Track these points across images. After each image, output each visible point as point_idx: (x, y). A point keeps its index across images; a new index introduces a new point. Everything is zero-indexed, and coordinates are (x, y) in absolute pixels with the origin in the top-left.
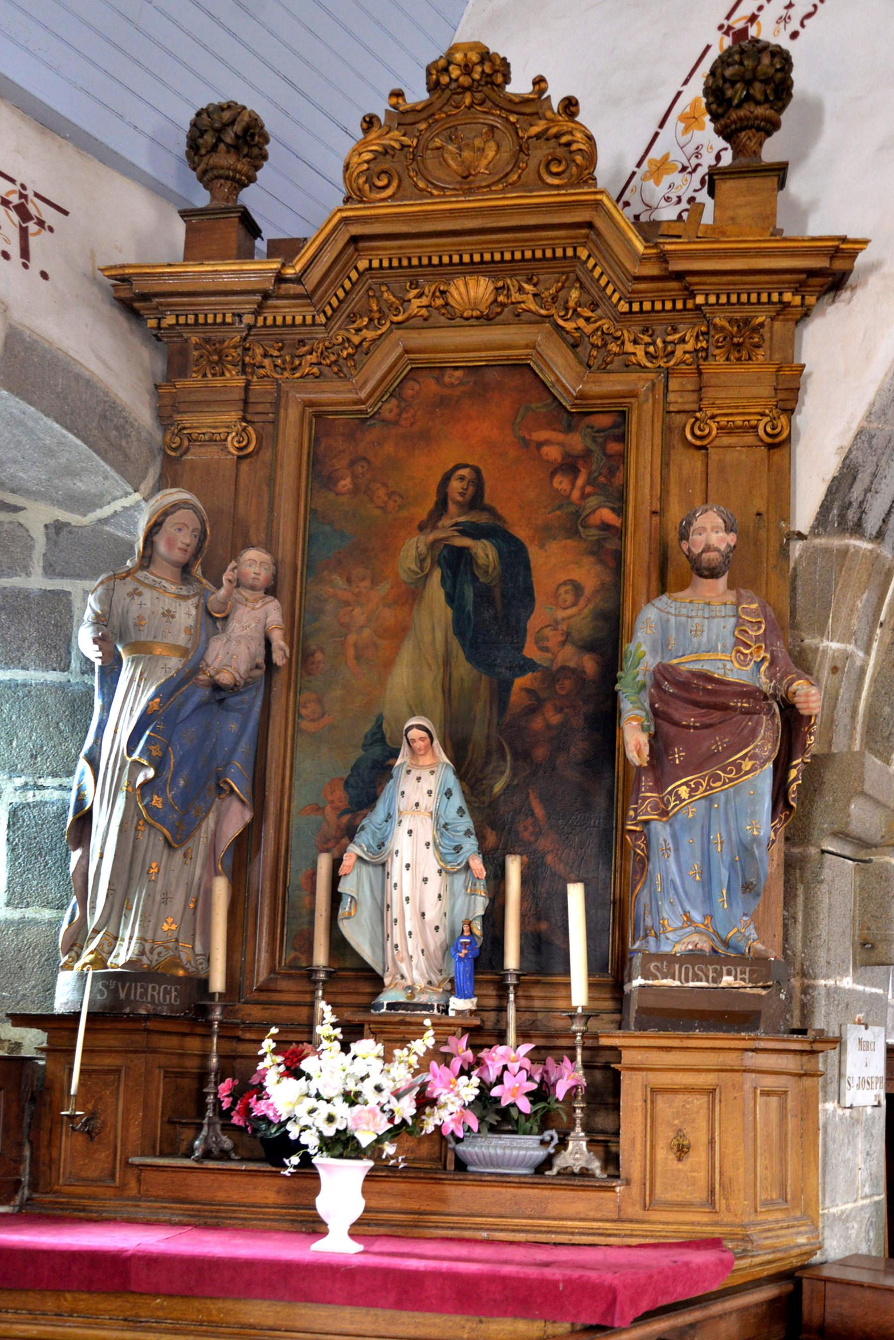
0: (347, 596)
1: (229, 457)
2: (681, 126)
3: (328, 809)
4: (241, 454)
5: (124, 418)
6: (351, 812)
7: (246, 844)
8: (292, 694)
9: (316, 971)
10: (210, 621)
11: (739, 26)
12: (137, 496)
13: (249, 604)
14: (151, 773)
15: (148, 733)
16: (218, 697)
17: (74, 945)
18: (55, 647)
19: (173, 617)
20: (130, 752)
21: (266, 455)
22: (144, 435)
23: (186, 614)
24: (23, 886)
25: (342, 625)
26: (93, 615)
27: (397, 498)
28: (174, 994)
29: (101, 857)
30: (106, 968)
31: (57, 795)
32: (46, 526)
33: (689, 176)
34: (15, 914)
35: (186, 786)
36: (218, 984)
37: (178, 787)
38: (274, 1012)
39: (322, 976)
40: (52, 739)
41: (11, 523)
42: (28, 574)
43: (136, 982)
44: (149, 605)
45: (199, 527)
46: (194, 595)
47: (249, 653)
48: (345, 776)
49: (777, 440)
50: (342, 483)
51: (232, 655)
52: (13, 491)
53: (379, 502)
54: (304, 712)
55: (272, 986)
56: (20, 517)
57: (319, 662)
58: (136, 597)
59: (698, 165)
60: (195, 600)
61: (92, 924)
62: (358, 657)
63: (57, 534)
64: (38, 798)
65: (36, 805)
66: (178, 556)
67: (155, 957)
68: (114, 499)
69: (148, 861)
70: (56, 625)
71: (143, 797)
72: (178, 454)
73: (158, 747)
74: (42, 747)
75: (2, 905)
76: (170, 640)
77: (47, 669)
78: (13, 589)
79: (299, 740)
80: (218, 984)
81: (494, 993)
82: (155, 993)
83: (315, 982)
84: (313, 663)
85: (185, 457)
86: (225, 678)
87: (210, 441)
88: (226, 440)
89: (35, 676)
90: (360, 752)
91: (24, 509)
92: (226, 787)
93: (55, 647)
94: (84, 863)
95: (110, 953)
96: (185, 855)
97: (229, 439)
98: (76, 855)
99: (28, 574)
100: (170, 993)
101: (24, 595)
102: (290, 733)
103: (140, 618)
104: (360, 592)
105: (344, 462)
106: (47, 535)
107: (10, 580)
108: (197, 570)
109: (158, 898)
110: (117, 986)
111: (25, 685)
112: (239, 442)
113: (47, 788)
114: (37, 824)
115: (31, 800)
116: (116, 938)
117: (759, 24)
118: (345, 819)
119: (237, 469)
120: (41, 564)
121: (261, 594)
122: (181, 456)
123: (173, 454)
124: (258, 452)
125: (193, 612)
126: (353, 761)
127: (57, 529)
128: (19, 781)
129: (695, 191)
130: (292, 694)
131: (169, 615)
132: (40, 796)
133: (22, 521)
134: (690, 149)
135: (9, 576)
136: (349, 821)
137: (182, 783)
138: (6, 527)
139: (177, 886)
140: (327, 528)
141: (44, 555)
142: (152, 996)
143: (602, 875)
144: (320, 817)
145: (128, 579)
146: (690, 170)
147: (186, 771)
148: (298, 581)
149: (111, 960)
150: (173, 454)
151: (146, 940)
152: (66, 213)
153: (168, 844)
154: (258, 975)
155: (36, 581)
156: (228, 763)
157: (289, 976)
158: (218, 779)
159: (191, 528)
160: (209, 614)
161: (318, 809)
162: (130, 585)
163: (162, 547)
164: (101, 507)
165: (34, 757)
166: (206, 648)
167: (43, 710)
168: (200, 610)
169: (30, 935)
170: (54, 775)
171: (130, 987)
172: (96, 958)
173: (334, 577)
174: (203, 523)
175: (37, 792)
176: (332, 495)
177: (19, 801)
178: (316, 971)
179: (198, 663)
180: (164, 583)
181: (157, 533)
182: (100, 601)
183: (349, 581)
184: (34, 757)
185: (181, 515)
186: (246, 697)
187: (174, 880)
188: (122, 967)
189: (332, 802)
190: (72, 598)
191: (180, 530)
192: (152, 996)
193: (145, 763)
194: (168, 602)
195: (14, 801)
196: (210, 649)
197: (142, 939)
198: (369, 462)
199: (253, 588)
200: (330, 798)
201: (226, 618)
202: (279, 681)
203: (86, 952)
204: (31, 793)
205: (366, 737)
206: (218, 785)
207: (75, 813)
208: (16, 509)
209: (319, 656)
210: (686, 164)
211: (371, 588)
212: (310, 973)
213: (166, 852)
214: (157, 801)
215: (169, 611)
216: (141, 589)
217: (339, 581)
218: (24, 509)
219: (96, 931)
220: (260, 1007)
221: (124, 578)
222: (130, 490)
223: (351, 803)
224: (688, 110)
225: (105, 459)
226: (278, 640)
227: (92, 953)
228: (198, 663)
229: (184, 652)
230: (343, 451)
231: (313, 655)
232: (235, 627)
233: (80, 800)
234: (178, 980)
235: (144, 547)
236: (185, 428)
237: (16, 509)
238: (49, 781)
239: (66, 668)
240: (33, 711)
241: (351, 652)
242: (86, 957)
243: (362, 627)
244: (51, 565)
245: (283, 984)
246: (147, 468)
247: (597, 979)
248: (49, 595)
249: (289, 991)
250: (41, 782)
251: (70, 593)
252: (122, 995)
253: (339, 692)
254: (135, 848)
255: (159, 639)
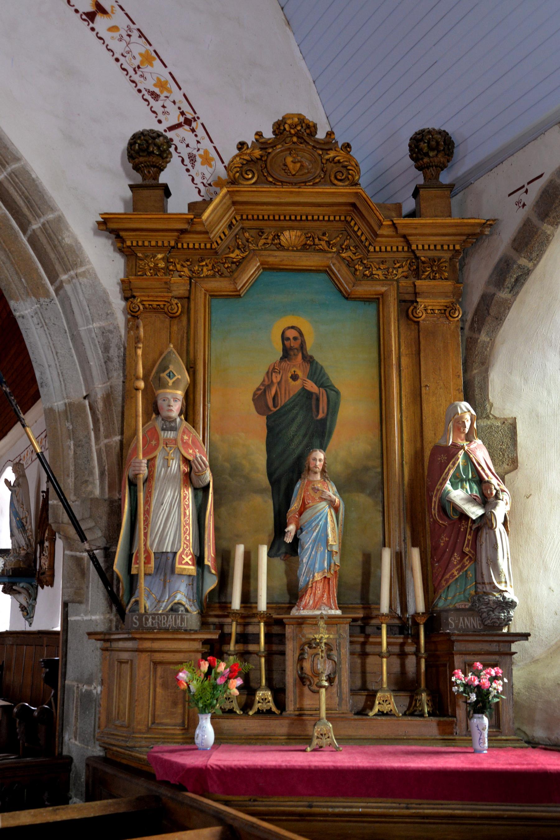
2: (163, 79)
11: (194, 125)
33: (134, 67)
49: (174, 315)
59: (136, 73)
81: (99, 389)
117: (189, 131)
129: (122, 64)
134: (147, 75)
143: (501, 762)
146: (137, 69)
152: (510, 195)
210: (140, 70)
224: (168, 86)
247: (243, 605)
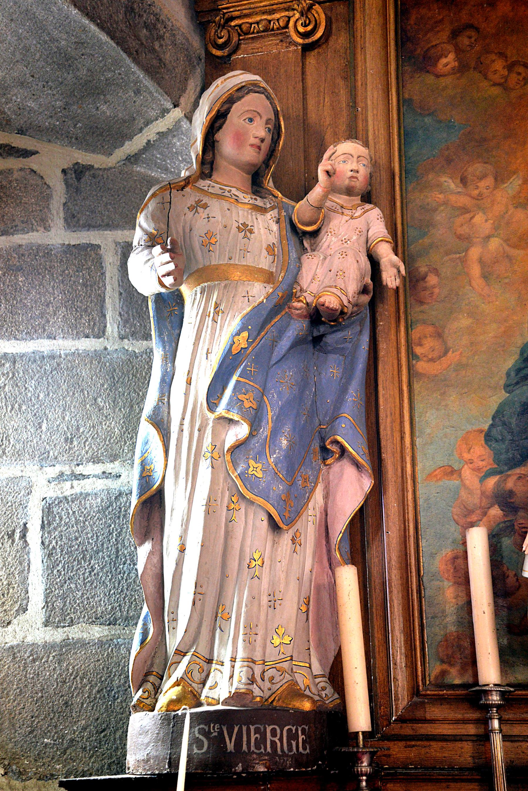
0: (464, 200)
1: (293, 48)
3: (467, 473)
4: (307, 41)
5: (155, 15)
6: (501, 472)
7: (364, 525)
8: (402, 329)
9: (487, 693)
10: (293, 240)
12: (177, 113)
13: (346, 212)
14: (242, 431)
15: (235, 378)
16: (316, 334)
17: (148, 674)
18: (86, 311)
19: (251, 231)
20: (212, 406)
21: (339, 41)
22: (179, 39)
23: (267, 228)
24: (64, 598)
25: (459, 237)
26: (145, 237)
27: (521, 69)
28: (301, 737)
29: (182, 550)
30: (200, 705)
31: (101, 484)
32: (64, 171)
34: (56, 635)
35: (291, 447)
36: (360, 719)
37: (280, 449)
38: (423, 751)
39: (495, 698)
40: (89, 419)
41: (21, 170)
42: (47, 229)
43: (248, 725)
44: (219, 218)
45: (273, 118)
46: (272, 208)
47: (359, 269)
48: (486, 427)
50: (444, 61)
51: (333, 274)
52: (21, 132)
53: (496, 78)
54: (418, 350)
55: (419, 714)
56: (32, 163)
57: (434, 287)
58: (200, 210)
60: (274, 213)
61: (173, 641)
62: (485, 276)
63: (79, 179)
64: (77, 490)
65: (75, 498)
66: (250, 155)
67: (267, 684)
68: (147, 123)
69: (247, 550)
70: (85, 285)
71: (235, 464)
72: (226, 52)
73: (250, 395)
74: (78, 429)
75: (40, 624)
76: (249, 261)
77: (78, 336)
78: (30, 246)
79: (416, 386)
80: (360, 719)
82: (276, 740)
83: (487, 707)
84: (425, 289)
85: (234, 57)
86: (331, 301)
87: (266, 30)
88: (286, 26)
89: (65, 345)
90: (502, 396)
91: (37, 152)
92: (334, 448)
93: (86, 311)
94: (155, 559)
95: (204, 683)
96: (293, 540)
97: (291, 24)
98: (144, 551)
99: (47, 229)
100: (295, 737)
101: (46, 252)
102: (405, 378)
103: (209, 235)
104: (480, 195)
105: (445, 35)
106: (66, 182)
107: (26, 236)
108: (269, 184)
109: (265, 600)
110: (221, 733)
111: (52, 357)
112: (305, 25)
113: (88, 477)
114: (77, 522)
115: (68, 493)
116: (210, 661)
118: (492, 482)
119: (303, 64)
120: (62, 215)
121: (357, 200)
122: (230, 55)
123: (219, 53)
124: (327, 41)
125: (275, 227)
126: (494, 407)
127: (77, 173)
128: (52, 472)
130: (402, 329)
131: (246, 229)
132: (79, 486)
133: (35, 167)
135: (24, 231)
136: (497, 484)
137: (284, 443)
138: (16, 175)
139: (287, 584)
140: (428, 120)
141: (64, 204)
142: (273, 743)
144: (457, 482)
145: (188, 189)
147: (287, 428)
148: (397, 188)
149: (205, 692)
150: (219, 53)
151: (254, 662)
153: (275, 527)
154: (397, 699)
155: (58, 235)
156: (335, 418)
157: (440, 700)
158: (323, 440)
159: (265, 119)
160: (293, 227)
161: (451, 472)
162: (190, 196)
163: (227, 145)
164: (131, 138)
165: (69, 441)
166: (299, 268)
167: (77, 385)
168: (283, 225)
169: (76, 660)
170: (95, 460)
171: (240, 731)
172: (184, 691)
173: (443, 179)
174: (277, 114)
175: (75, 483)
176: (430, 79)
177: (54, 495)
178: (487, 693)
179: (291, 287)
180: (234, 191)
181: (220, 127)
182: (154, 218)
183: (464, 181)
184: (69, 441)
185: (253, 101)
186: (348, 333)
187: (283, 576)
188: (225, 702)
189: (471, 462)
190: (102, 252)
191: (251, 120)
192: (273, 743)
193: (236, 418)
194: (242, 214)
195: (48, 495)
196: (304, 270)
197: (251, 661)
198: (477, 30)
199: (349, 191)
200: (467, 456)
201: (315, 234)
202: (387, 310)
203: (167, 684)
204: (68, 484)
205: (508, 375)
206: (324, 450)
207: (140, 495)
208: (26, 153)
209: (432, 280)
211: (496, 187)
212: (473, 695)
213: (270, 537)
214: (256, 469)
215: (244, 224)
216: (205, 200)
217: (450, 183)
218: (37, 152)
219: (181, 653)
220: (401, 744)
221: (182, 189)
222: (169, 105)
223: (497, 460)
225: (136, 61)
226: (386, 254)
227: (177, 684)
228: (291, 287)
229: (269, 278)
230: (441, 21)
231: (424, 278)
232: (329, 241)
233: (145, 478)
234: (301, 717)
235: (204, 151)
236: (232, 19)
237: (26, 153)
238: (89, 469)
239: (101, 333)
240: (64, 387)
241: (476, 270)
242: (169, 693)
243: (488, 237)
244: (74, 216)
245: (435, 711)
246: (186, 80)
248: (75, 250)
249: (444, 721)
250: (79, 470)
251: (99, 246)
252: (230, 746)
253: (465, 322)
254: (228, 534)
255: (235, 261)
